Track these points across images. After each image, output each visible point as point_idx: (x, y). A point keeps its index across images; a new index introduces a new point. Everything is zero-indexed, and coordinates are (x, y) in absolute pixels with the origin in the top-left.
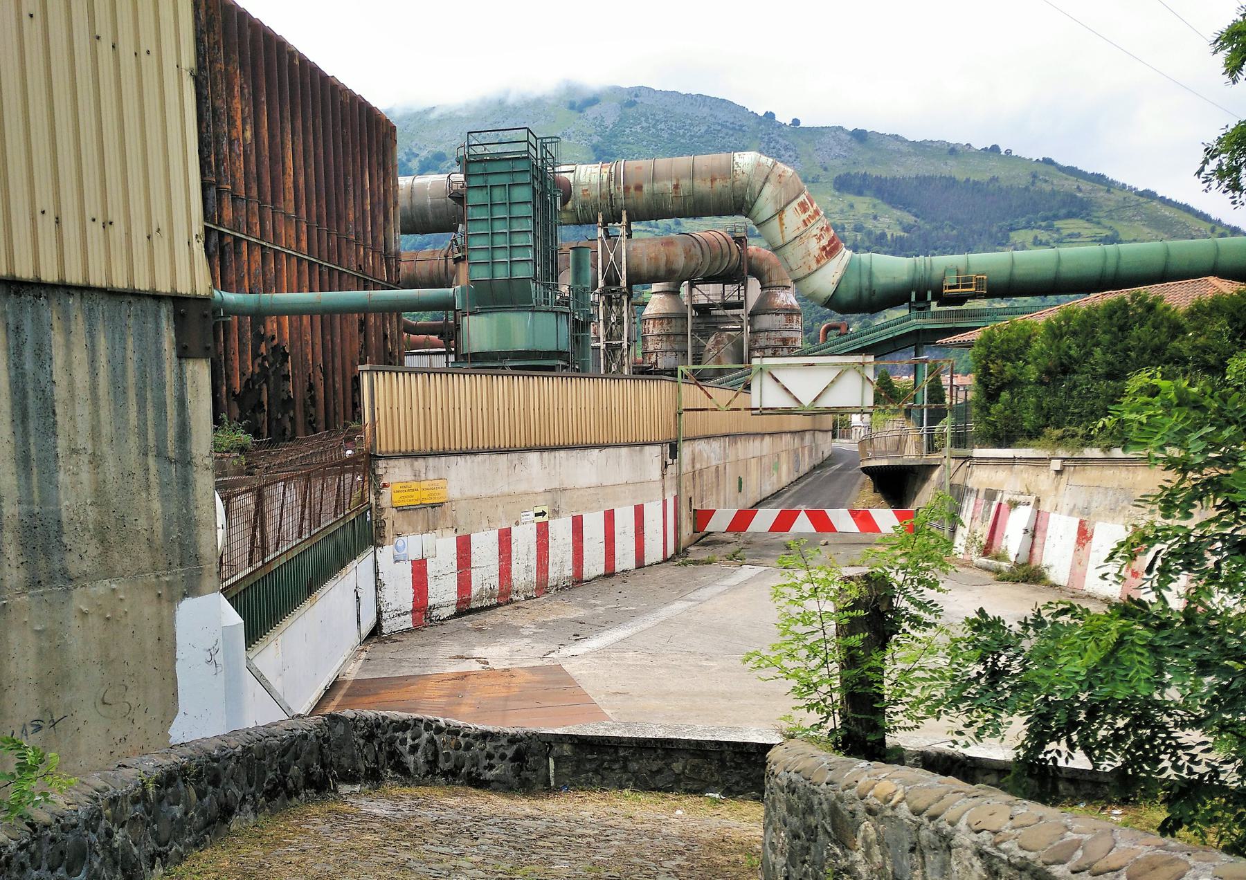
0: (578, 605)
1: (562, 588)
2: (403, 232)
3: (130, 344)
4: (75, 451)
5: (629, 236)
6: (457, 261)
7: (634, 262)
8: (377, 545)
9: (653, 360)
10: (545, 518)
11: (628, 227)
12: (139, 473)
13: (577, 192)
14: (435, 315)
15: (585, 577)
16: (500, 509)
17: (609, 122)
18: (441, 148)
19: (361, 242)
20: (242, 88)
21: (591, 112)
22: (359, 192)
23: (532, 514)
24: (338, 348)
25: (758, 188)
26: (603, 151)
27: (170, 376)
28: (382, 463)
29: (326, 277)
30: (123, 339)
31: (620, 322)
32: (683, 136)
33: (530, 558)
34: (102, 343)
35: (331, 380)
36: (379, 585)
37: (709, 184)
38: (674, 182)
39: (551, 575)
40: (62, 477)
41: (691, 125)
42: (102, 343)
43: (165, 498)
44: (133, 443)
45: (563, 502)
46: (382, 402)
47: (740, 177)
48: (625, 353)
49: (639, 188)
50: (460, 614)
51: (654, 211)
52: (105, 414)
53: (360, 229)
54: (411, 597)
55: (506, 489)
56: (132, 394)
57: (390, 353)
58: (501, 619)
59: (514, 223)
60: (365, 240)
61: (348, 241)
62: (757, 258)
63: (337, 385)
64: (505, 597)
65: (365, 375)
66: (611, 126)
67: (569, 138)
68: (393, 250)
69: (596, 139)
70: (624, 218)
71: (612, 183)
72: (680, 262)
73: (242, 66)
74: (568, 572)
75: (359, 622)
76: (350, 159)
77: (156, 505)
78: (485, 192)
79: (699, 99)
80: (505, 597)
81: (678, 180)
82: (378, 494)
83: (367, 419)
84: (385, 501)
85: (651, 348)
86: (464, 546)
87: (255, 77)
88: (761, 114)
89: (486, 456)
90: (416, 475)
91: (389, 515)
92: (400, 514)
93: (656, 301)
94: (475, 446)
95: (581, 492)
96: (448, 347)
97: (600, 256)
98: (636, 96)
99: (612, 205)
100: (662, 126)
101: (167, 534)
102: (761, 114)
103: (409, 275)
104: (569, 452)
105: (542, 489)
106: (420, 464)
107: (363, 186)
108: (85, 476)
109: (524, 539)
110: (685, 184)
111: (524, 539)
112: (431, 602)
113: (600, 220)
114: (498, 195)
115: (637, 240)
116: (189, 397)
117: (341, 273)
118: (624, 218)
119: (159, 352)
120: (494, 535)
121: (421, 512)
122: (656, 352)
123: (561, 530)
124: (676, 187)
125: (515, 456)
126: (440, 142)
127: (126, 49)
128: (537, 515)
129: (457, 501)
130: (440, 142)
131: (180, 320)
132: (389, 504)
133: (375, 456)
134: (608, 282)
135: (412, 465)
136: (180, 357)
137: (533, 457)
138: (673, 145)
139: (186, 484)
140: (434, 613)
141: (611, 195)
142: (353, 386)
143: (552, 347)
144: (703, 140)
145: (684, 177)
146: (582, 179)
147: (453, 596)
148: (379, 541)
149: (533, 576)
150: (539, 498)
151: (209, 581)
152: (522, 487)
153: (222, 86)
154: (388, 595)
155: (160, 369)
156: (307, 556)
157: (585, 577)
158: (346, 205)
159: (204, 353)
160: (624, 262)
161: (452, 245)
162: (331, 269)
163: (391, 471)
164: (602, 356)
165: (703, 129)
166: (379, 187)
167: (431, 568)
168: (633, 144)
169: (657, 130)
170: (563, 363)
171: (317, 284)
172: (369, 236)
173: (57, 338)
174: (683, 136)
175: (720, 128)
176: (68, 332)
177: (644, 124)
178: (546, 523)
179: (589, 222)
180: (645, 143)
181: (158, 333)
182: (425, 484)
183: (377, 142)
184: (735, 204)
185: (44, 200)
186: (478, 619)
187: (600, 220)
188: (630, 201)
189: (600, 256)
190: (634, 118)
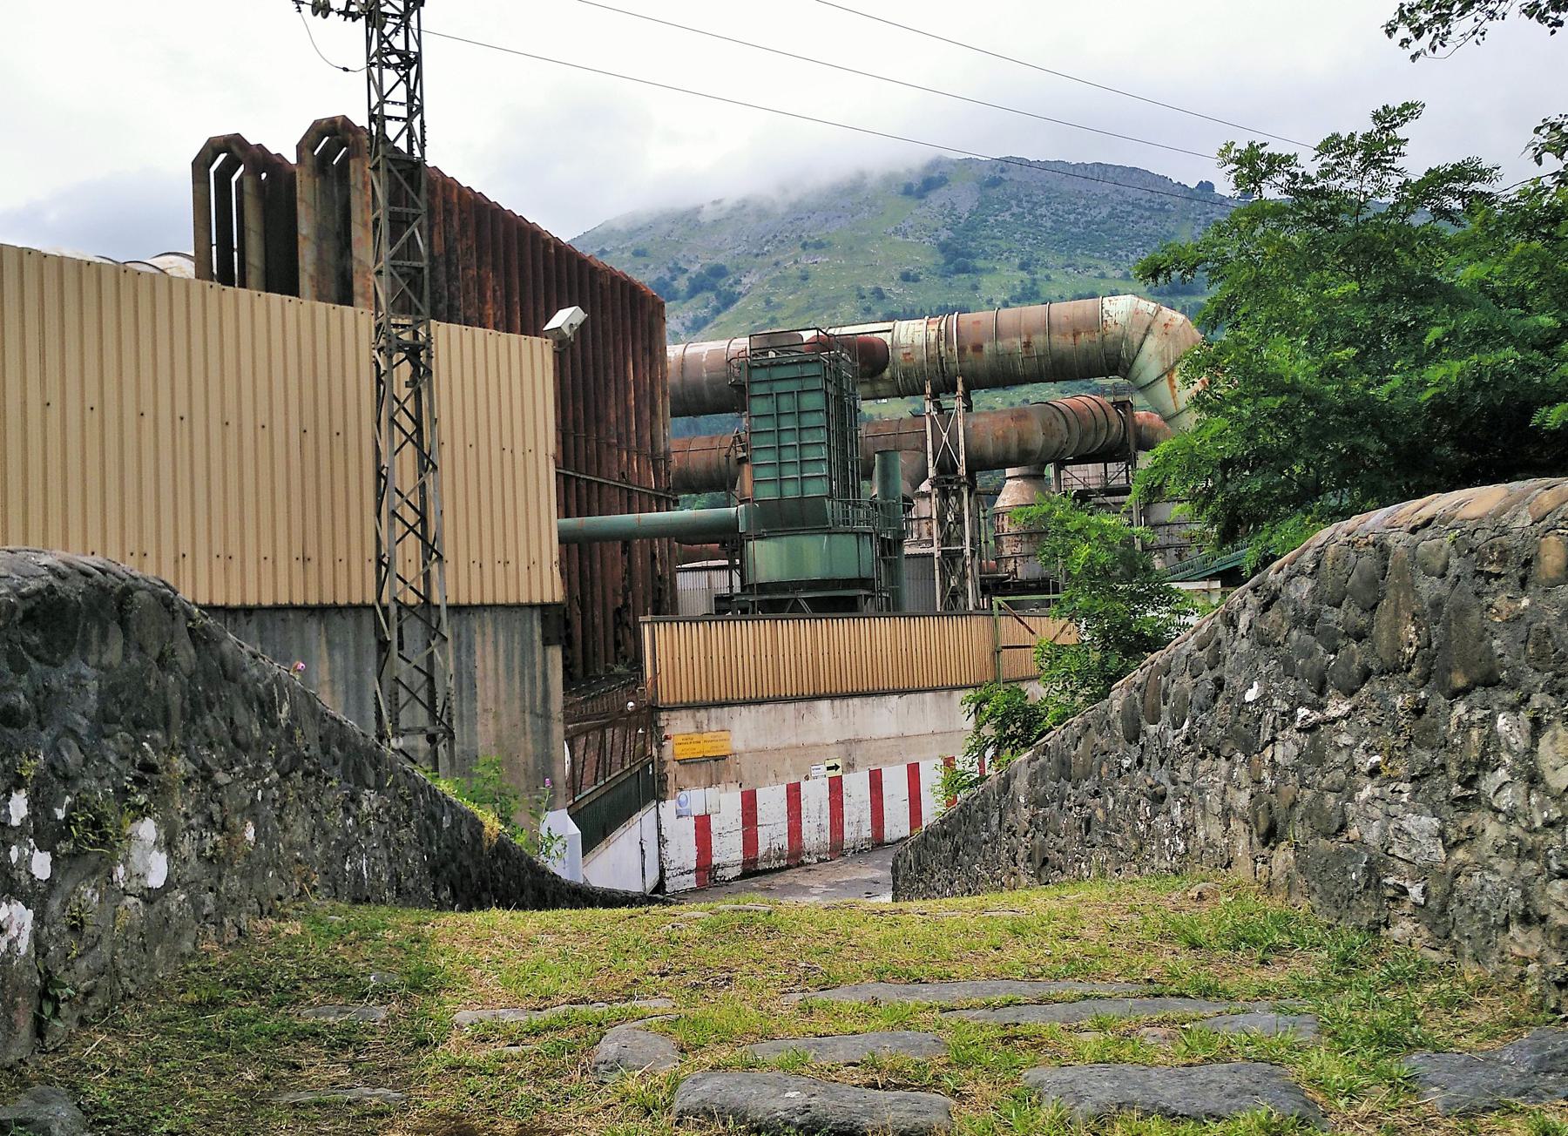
0: (877, 866)
1: (860, 851)
2: (672, 416)
3: (517, 637)
4: (485, 711)
5: (969, 408)
6: (742, 461)
7: (976, 442)
8: (661, 798)
9: (1011, 567)
10: (839, 772)
11: (966, 397)
12: (520, 725)
13: (897, 356)
14: (713, 498)
15: (887, 839)
16: (788, 762)
17: (964, 209)
18: (720, 260)
19: (624, 446)
20: (494, 291)
21: (936, 198)
22: (621, 386)
23: (823, 768)
24: (598, 574)
25: (1136, 344)
26: (956, 251)
27: (538, 658)
28: (664, 715)
29: (584, 492)
30: (513, 636)
31: (959, 520)
32: (1075, 223)
33: (823, 816)
34: (501, 638)
35: (589, 614)
36: (662, 841)
37: (1071, 339)
38: (1024, 339)
39: (846, 836)
40: (479, 728)
41: (1086, 206)
42: (501, 638)
43: (535, 741)
44: (517, 704)
45: (858, 754)
46: (663, 649)
47: (1112, 329)
48: (968, 562)
49: (978, 348)
50: (746, 875)
51: (1003, 376)
52: (502, 685)
53: (622, 430)
54: (694, 855)
55: (794, 741)
56: (517, 671)
57: (660, 578)
58: (790, 880)
59: (805, 434)
60: (629, 440)
61: (609, 445)
62: (1148, 428)
63: (597, 620)
64: (795, 858)
65: (646, 626)
66: (966, 215)
67: (905, 235)
68: (662, 450)
69: (944, 235)
70: (960, 387)
71: (942, 343)
72: (1037, 441)
73: (495, 268)
74: (867, 833)
75: (644, 875)
76: (611, 349)
77: (530, 746)
78: (770, 400)
79: (1096, 169)
80: (795, 858)
81: (1029, 336)
82: (660, 746)
83: (649, 674)
84: (667, 754)
85: (1007, 552)
86: (749, 803)
87: (508, 274)
88: (1192, 185)
89: (771, 706)
90: (699, 728)
91: (672, 768)
92: (682, 767)
93: (1012, 492)
94: (760, 695)
95: (879, 743)
96: (732, 561)
97: (929, 437)
98: (1002, 171)
99: (943, 372)
100: (1043, 210)
101: (536, 766)
102: (1192, 185)
103: (680, 469)
104: (864, 699)
105: (835, 741)
106: (702, 715)
107: (626, 377)
108: (491, 727)
109: (815, 795)
110: (1039, 340)
111: (815, 795)
112: (715, 861)
113: (928, 390)
114: (786, 403)
115: (978, 414)
116: (549, 672)
117: (600, 484)
118: (960, 387)
119: (532, 641)
120: (781, 791)
121: (704, 765)
122: (1014, 557)
123: (857, 786)
124: (1027, 345)
125: (803, 705)
126: (717, 251)
127: (518, 454)
128: (829, 768)
129: (741, 754)
130: (717, 251)
131: (544, 620)
132: (671, 757)
133: (656, 707)
134: (941, 469)
135: (694, 717)
136: (544, 645)
137: (824, 705)
138: (1060, 236)
139: (547, 732)
140: (719, 873)
141: (941, 359)
142: (615, 620)
143: (853, 574)
144: (1106, 227)
145: (1037, 331)
146: (903, 340)
147: (738, 856)
148: (661, 795)
149: (826, 836)
150: (832, 750)
151: (561, 801)
152: (811, 739)
153: (474, 294)
154: (671, 851)
155: (533, 653)
156: (603, 799)
157: (887, 839)
158: (606, 402)
159: (558, 641)
160: (962, 444)
161: (734, 442)
162: (589, 482)
163: (672, 723)
164: (937, 567)
165: (1105, 212)
166: (644, 375)
167: (715, 824)
168: (1001, 239)
169: (1035, 217)
170: (867, 593)
171: (573, 509)
172: (633, 436)
173: (478, 639)
174: (1075, 223)
175: (1130, 208)
176: (484, 634)
177: (1015, 210)
178: (840, 778)
179: (914, 393)
180: (1017, 236)
181: (532, 630)
182: (707, 736)
183: (642, 322)
184: (1107, 364)
185: (474, 555)
186: (766, 880)
187: (928, 390)
188: (967, 365)
189: (929, 437)
190: (1001, 202)
